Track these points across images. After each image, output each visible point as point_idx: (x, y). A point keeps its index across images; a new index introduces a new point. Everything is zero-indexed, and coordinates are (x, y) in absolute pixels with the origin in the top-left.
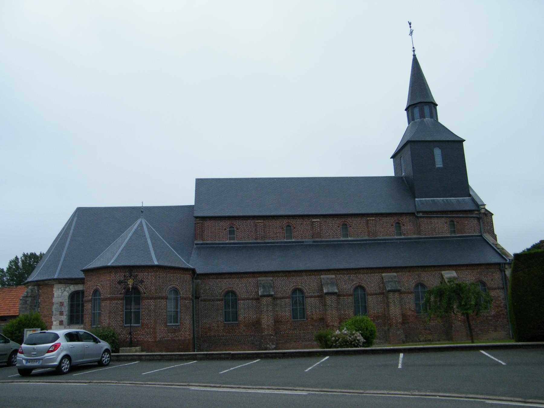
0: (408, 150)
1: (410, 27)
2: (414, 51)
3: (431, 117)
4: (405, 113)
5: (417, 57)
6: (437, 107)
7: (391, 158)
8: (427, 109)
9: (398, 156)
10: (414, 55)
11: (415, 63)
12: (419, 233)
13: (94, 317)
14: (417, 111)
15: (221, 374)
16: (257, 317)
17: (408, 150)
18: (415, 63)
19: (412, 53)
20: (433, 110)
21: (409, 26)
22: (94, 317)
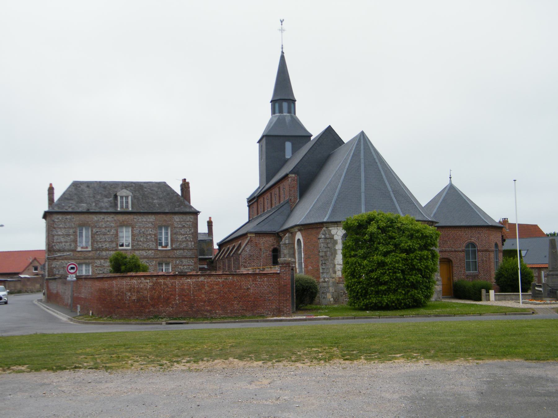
0: (264, 139)
1: (282, 24)
2: (282, 48)
3: (289, 112)
4: (270, 104)
5: (285, 55)
6: (296, 102)
7: (258, 142)
8: (285, 105)
9: (261, 142)
10: (283, 53)
11: (282, 58)
12: (129, 237)
13: (281, 207)
14: (277, 105)
15: (29, 275)
16: (173, 285)
17: (264, 139)
18: (282, 58)
19: (281, 50)
20: (292, 105)
21: (281, 23)
22: (281, 207)
